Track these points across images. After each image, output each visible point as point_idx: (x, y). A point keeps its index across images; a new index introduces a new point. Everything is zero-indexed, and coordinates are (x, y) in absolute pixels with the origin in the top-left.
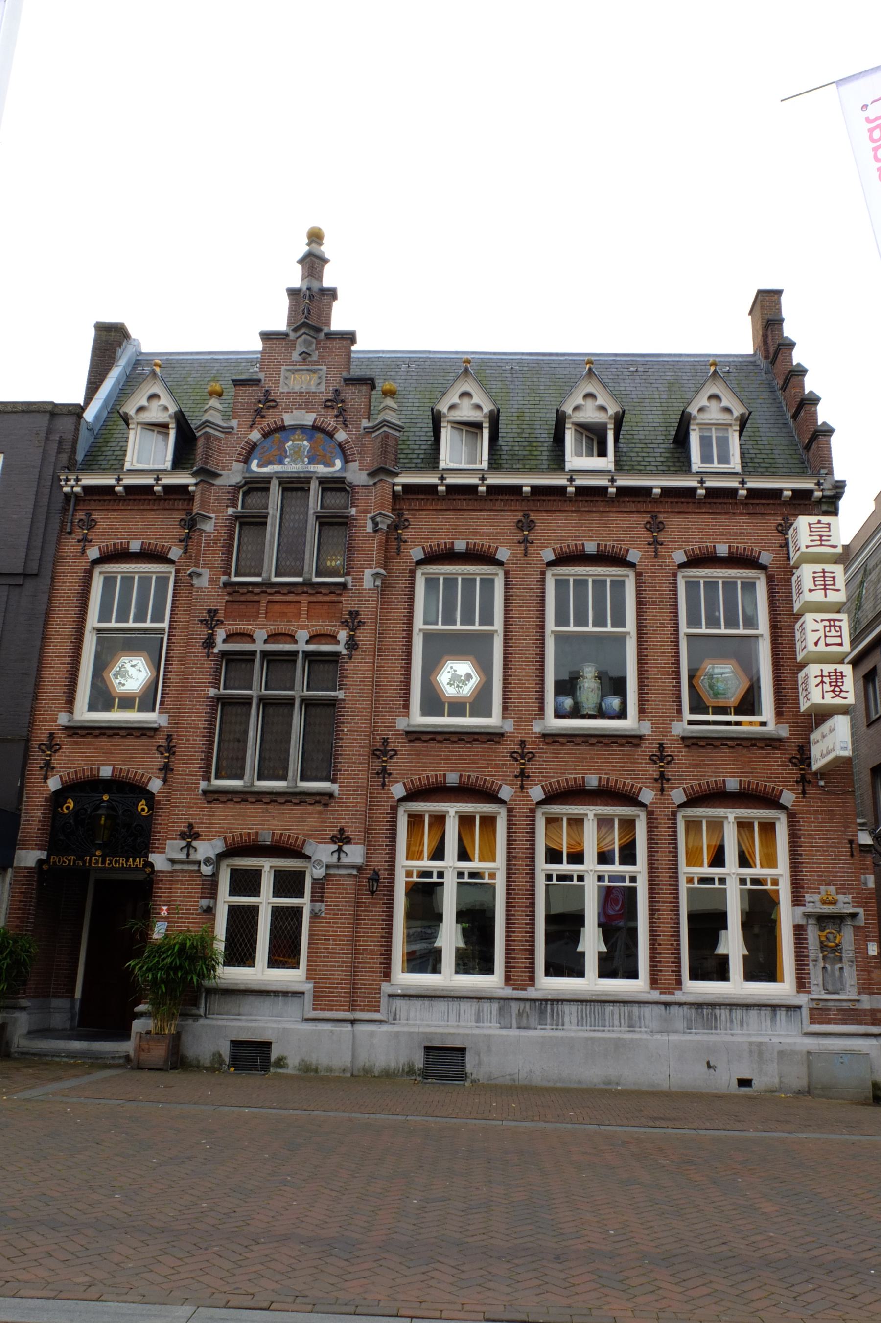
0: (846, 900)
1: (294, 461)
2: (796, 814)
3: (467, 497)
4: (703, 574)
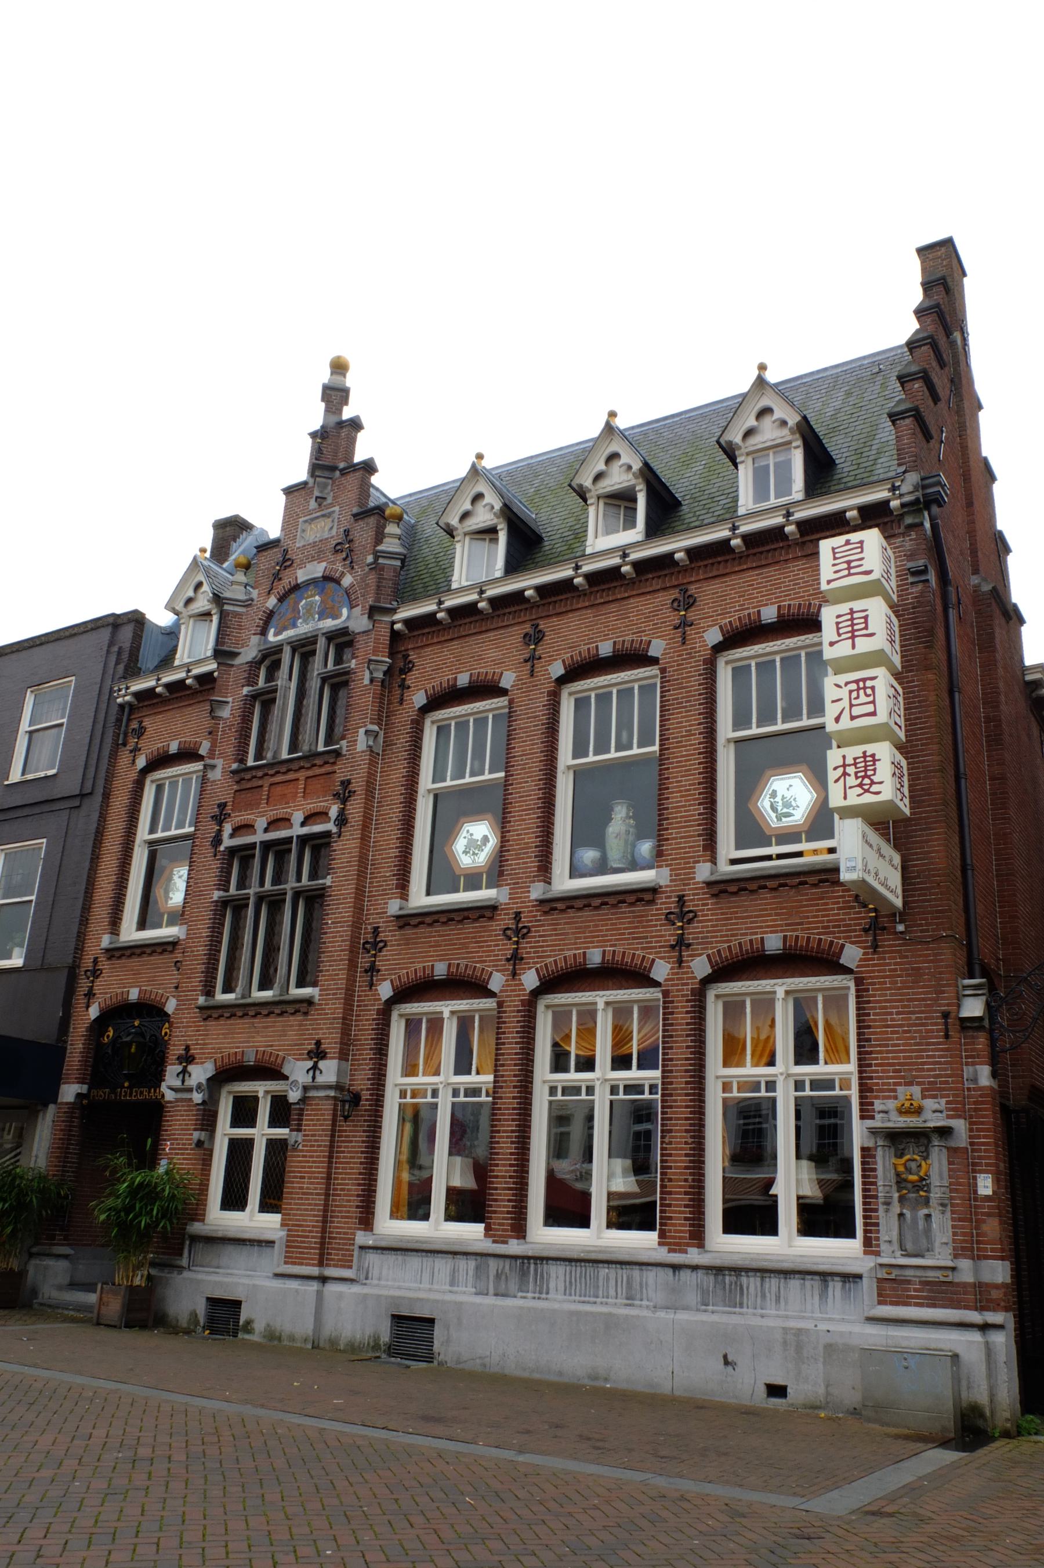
0: (936, 1106)
1: (306, 621)
2: (863, 978)
3: (472, 619)
4: (752, 653)
